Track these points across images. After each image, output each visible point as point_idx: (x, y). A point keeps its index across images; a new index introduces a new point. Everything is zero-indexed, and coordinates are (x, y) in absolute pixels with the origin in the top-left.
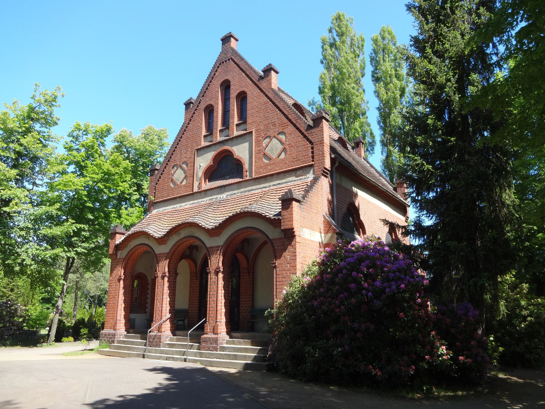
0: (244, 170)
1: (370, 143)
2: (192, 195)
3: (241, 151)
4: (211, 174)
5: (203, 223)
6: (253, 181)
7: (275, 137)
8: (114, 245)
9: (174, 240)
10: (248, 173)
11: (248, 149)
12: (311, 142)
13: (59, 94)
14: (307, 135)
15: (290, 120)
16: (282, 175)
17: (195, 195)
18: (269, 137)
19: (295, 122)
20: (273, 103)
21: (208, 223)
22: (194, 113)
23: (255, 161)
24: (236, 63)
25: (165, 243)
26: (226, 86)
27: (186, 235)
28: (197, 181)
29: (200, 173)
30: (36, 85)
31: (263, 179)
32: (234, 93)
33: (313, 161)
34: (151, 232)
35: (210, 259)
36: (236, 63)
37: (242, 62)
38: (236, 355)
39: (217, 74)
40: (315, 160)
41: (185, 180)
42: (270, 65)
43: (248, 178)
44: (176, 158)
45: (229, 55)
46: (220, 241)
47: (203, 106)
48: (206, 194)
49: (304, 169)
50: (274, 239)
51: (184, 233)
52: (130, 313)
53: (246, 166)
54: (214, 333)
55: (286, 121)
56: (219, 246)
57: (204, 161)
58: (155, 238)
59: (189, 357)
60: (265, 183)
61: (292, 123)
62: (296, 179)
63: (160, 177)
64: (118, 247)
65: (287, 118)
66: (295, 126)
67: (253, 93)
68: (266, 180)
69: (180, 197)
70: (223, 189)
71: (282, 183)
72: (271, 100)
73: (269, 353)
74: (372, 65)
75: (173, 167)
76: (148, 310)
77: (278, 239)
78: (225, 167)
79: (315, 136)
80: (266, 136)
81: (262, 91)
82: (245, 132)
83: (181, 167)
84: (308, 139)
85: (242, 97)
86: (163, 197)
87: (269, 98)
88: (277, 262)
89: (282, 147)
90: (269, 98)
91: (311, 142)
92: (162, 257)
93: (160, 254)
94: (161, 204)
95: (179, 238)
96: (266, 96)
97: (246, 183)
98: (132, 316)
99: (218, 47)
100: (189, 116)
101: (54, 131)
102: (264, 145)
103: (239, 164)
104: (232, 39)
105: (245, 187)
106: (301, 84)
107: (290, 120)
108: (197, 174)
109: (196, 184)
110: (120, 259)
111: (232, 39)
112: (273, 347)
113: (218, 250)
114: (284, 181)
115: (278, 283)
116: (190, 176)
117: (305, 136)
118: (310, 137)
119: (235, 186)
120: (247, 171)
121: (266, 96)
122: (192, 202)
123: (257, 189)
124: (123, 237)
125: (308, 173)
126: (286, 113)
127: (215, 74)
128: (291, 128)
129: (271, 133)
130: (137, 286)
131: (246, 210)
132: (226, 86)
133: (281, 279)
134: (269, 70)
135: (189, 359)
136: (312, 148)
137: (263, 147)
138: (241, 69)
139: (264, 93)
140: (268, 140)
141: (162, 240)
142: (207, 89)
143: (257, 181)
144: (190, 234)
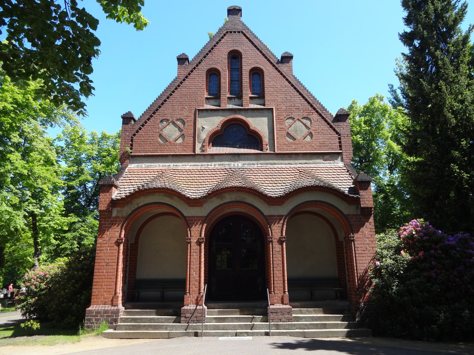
0: (264, 143)
2: (193, 157)
4: (217, 139)
6: (275, 156)
7: (299, 120)
8: (108, 201)
9: (216, 202)
10: (268, 146)
11: (267, 124)
12: (337, 133)
14: (334, 126)
16: (308, 156)
17: (197, 157)
18: (293, 119)
19: (320, 112)
22: (192, 71)
23: (277, 138)
27: (234, 200)
28: (199, 142)
29: (204, 135)
31: (287, 156)
33: (341, 150)
35: (270, 227)
38: (325, 324)
39: (223, 40)
40: (343, 149)
41: (181, 138)
43: (268, 152)
44: (166, 111)
46: (284, 210)
47: (204, 67)
48: (213, 158)
53: (266, 140)
54: (112, 305)
55: (310, 108)
56: (282, 216)
57: (209, 125)
59: (271, 331)
60: (290, 160)
62: (324, 162)
63: (140, 129)
64: (114, 203)
65: (312, 106)
66: (320, 115)
67: (270, 74)
68: (290, 157)
69: (173, 156)
70: (237, 157)
71: (310, 163)
73: (357, 319)
75: (162, 121)
77: (353, 215)
78: (235, 134)
79: (342, 129)
80: (288, 117)
82: (262, 107)
83: (174, 123)
85: (257, 73)
86: (147, 151)
88: (356, 235)
89: (307, 130)
91: (337, 133)
92: (195, 220)
94: (143, 159)
95: (222, 202)
97: (266, 156)
99: (223, 17)
105: (265, 160)
108: (198, 135)
109: (198, 146)
110: (117, 217)
112: (361, 314)
113: (281, 220)
114: (311, 161)
115: (357, 255)
117: (331, 127)
119: (252, 156)
120: (267, 145)
122: (192, 164)
123: (281, 164)
125: (337, 159)
129: (294, 115)
133: (360, 252)
134: (287, 58)
135: (272, 332)
136: (340, 139)
137: (286, 126)
140: (291, 121)
143: (279, 156)
144: (238, 199)
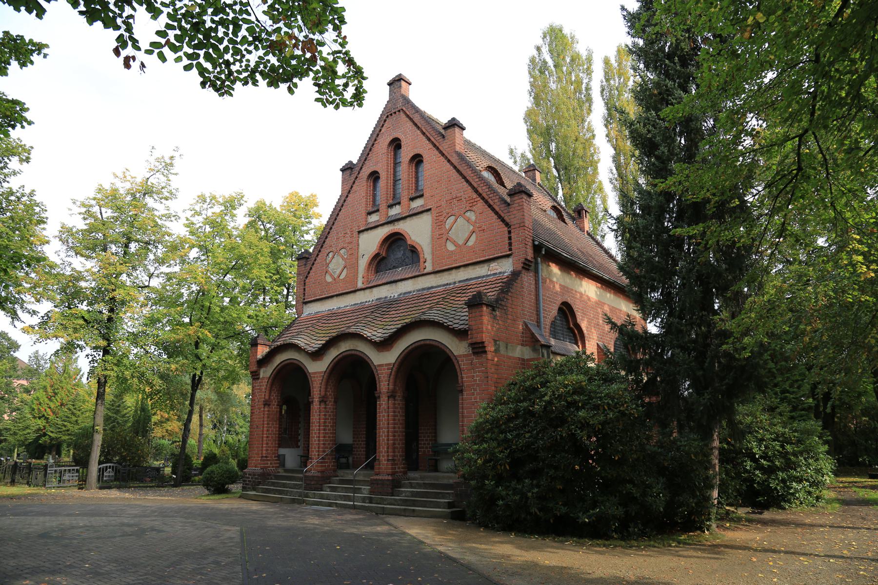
1: (721, 41)
3: (418, 231)
4: (379, 263)
5: (367, 333)
12: (507, 225)
13: (176, 154)
15: (480, 195)
19: (486, 197)
20: (458, 171)
21: (375, 333)
24: (408, 116)
25: (321, 359)
26: (396, 144)
30: (153, 148)
32: (406, 154)
34: (302, 344)
36: (408, 116)
37: (416, 115)
39: (383, 130)
42: (454, 119)
45: (399, 105)
49: (499, 261)
50: (460, 356)
51: (345, 347)
52: (279, 447)
55: (475, 196)
57: (370, 243)
58: (307, 353)
61: (483, 198)
65: (476, 191)
72: (455, 167)
74: (602, 96)
76: (301, 444)
77: (464, 356)
81: (443, 155)
84: (503, 220)
85: (417, 160)
87: (452, 164)
90: (452, 164)
93: (315, 373)
96: (449, 161)
98: (282, 451)
100: (348, 187)
101: (175, 206)
102: (447, 227)
103: (414, 252)
104: (403, 83)
106: (500, 133)
107: (480, 195)
110: (263, 378)
111: (403, 83)
116: (351, 265)
118: (506, 218)
121: (449, 161)
124: (267, 350)
126: (475, 185)
127: (380, 130)
128: (481, 203)
130: (286, 411)
131: (423, 317)
132: (396, 144)
136: (510, 232)
138: (416, 125)
139: (446, 158)
141: (317, 355)
142: (370, 150)
